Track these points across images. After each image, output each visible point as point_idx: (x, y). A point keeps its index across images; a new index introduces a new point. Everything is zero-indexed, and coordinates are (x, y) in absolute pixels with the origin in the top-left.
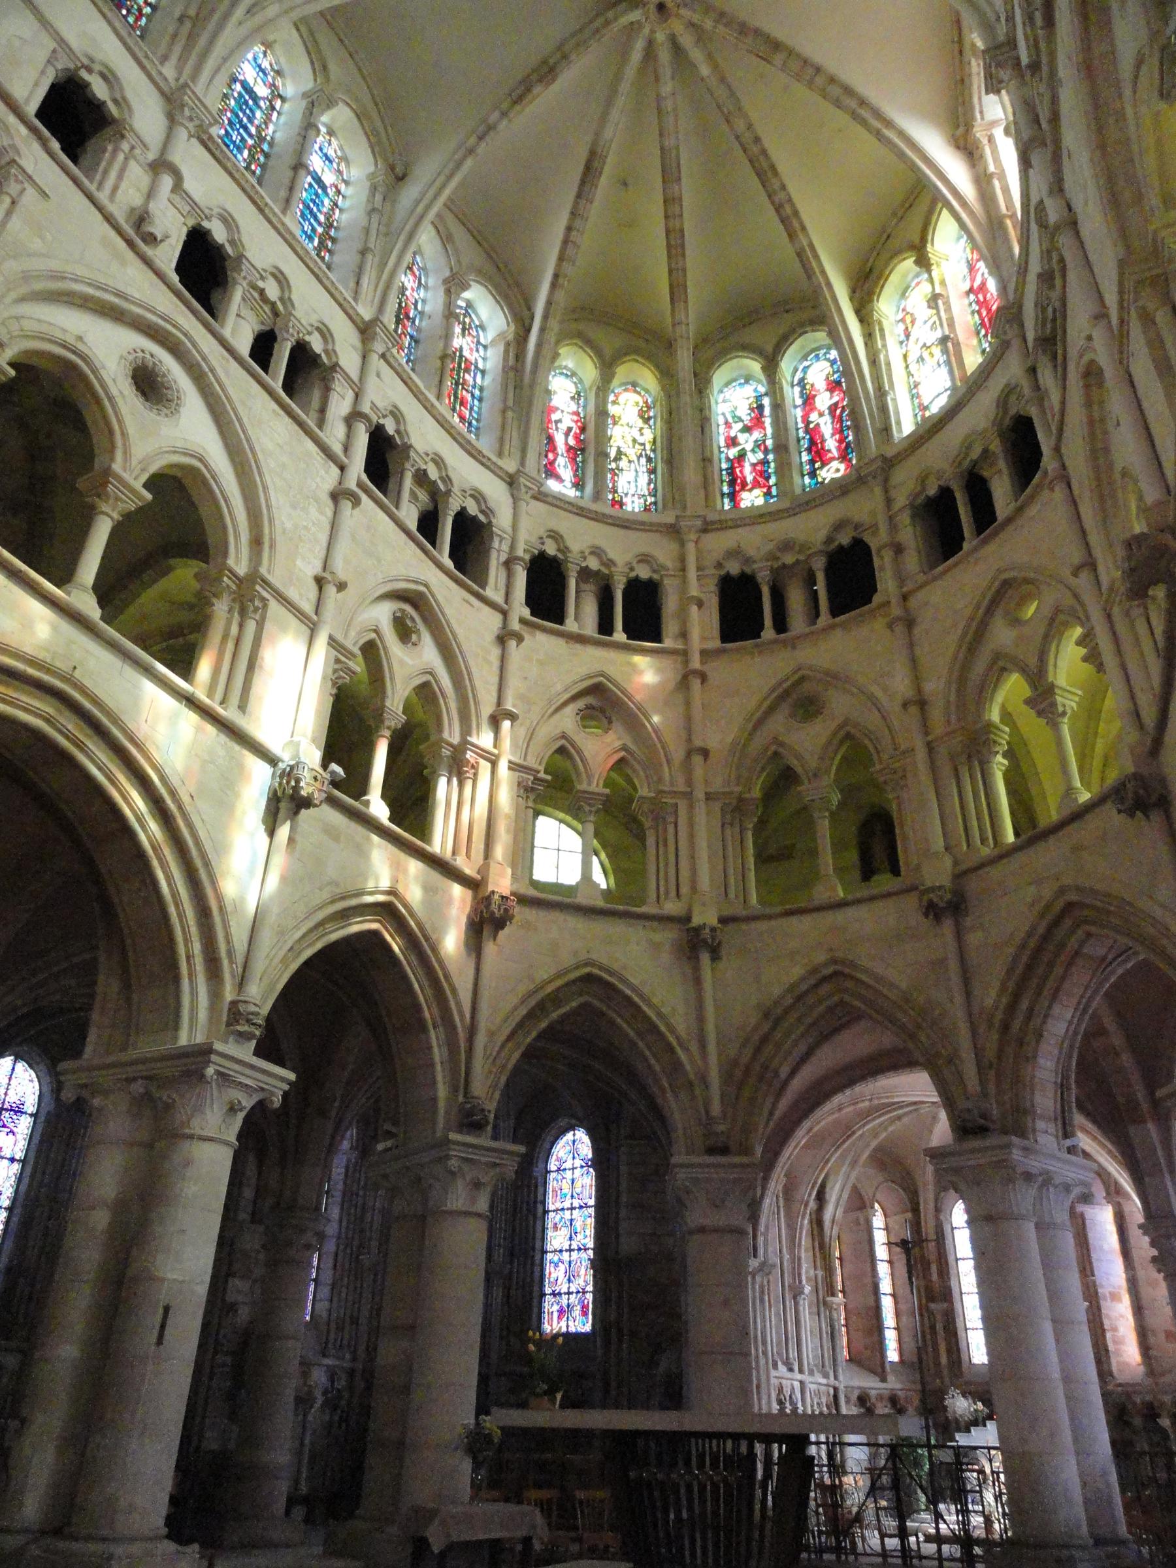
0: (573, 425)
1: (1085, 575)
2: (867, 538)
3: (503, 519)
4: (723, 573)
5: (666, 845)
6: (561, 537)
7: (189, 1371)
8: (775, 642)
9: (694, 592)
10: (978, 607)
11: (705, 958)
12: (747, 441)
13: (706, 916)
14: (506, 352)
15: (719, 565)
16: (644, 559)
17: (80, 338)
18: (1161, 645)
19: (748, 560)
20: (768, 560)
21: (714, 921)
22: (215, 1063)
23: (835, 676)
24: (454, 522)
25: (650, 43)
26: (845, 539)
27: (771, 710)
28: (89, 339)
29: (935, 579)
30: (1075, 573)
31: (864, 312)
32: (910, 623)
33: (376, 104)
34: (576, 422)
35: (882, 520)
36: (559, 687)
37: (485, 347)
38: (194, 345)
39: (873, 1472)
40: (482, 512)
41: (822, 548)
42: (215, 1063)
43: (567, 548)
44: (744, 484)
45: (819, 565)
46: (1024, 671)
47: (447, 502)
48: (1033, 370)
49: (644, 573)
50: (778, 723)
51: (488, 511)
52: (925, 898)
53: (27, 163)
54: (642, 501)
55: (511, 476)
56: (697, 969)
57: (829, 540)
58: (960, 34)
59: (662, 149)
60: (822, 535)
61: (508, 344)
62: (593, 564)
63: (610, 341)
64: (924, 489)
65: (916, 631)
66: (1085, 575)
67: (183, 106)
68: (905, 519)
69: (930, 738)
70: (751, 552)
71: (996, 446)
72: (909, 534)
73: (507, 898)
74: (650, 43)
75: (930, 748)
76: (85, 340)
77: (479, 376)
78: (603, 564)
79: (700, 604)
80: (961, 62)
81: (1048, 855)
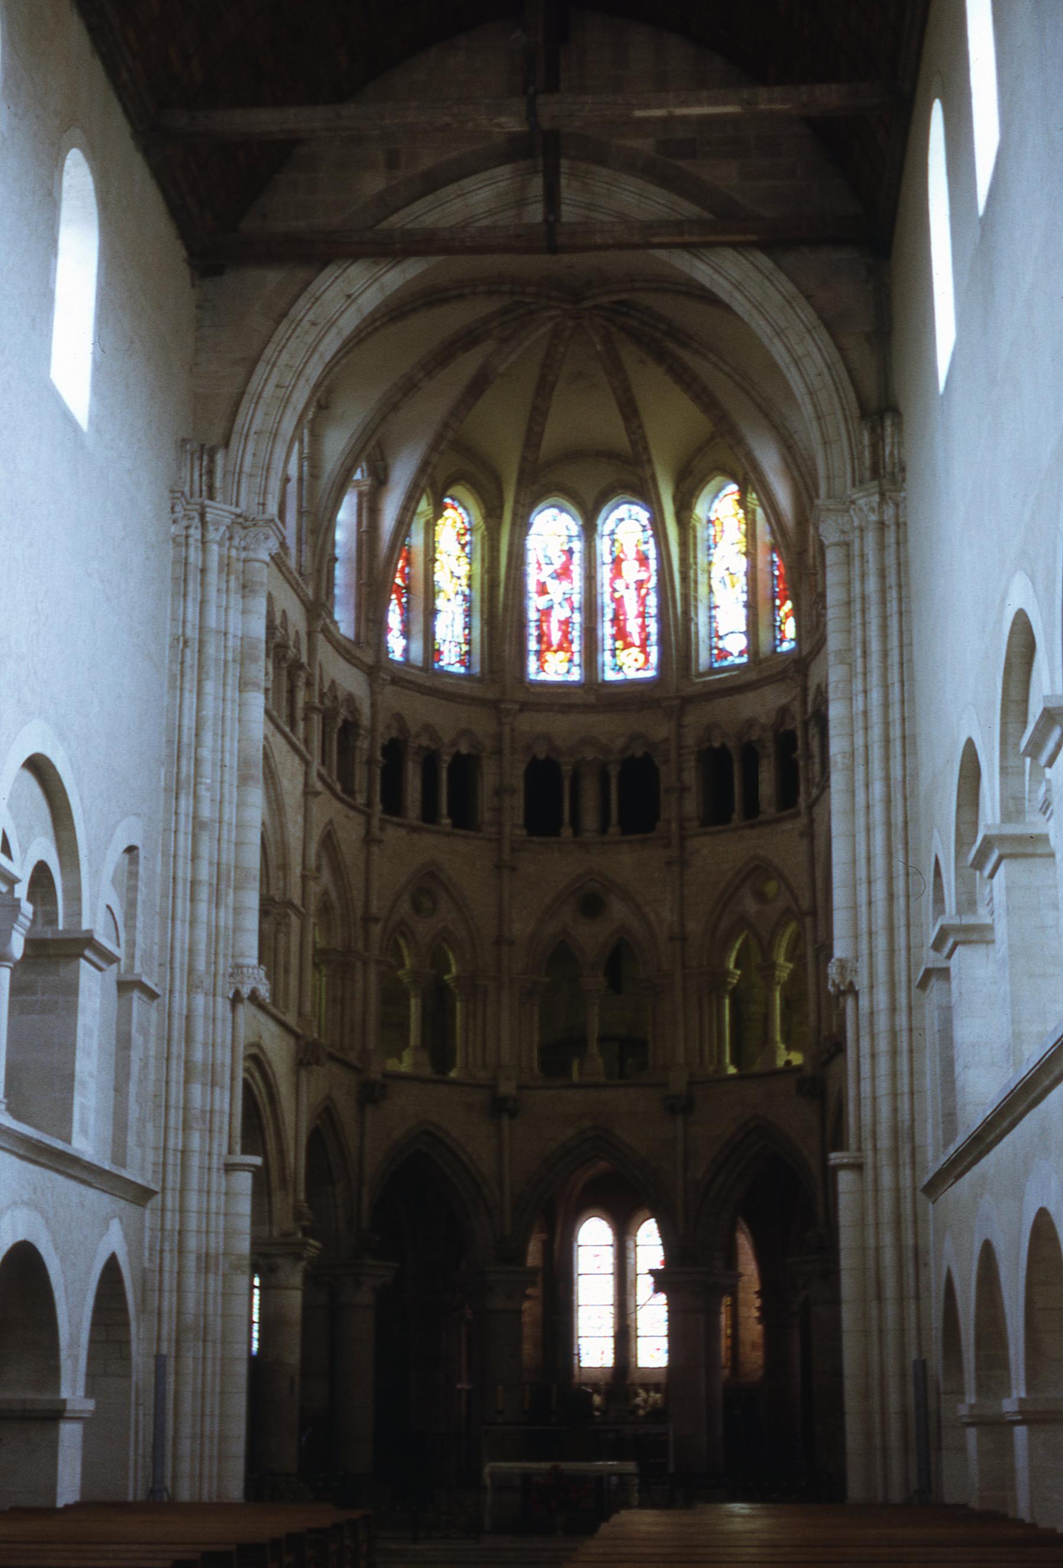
11: (505, 1119)
12: (557, 589)
13: (507, 1088)
16: (465, 733)
18: (935, 832)
39: (855, 617)
44: (549, 645)
45: (614, 771)
54: (458, 649)
55: (371, 668)
60: (620, 743)
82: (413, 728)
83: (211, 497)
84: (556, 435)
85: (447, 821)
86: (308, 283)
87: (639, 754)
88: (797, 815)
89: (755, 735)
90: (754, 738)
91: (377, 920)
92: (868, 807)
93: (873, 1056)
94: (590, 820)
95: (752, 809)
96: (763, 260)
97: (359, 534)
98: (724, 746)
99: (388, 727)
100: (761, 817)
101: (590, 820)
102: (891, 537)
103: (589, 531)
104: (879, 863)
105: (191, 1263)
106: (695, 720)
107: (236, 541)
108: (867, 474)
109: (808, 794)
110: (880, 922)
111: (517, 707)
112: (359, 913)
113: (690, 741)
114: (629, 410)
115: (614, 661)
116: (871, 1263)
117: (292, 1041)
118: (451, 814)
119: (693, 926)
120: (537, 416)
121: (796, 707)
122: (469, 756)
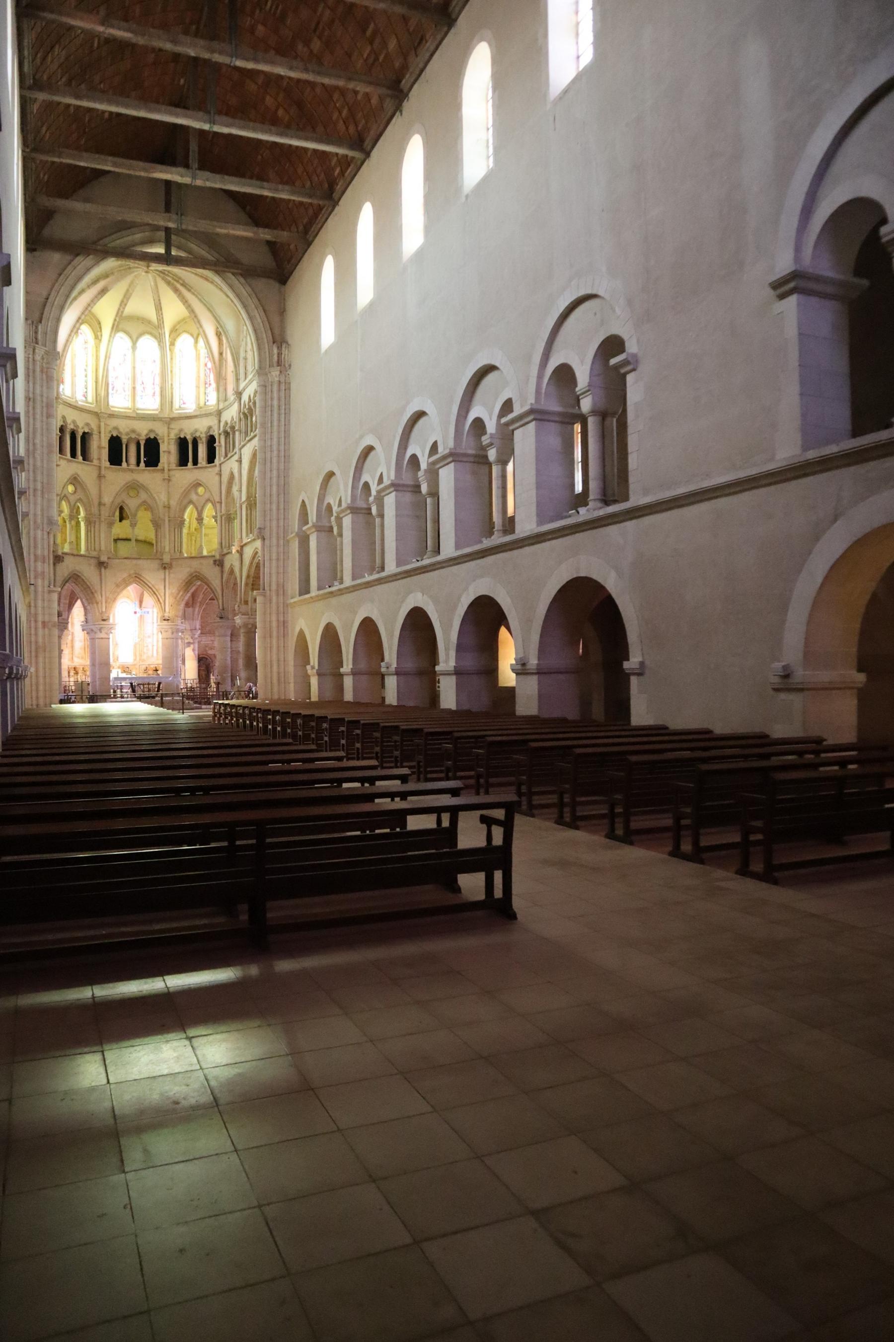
5: (91, 532)
7: (497, 555)
10: (189, 486)
11: (103, 570)
13: (104, 558)
15: (110, 431)
16: (87, 424)
19: (120, 433)
23: (144, 487)
29: (179, 470)
31: (172, 344)
32: (169, 480)
45: (142, 443)
50: (124, 496)
56: (100, 571)
57: (147, 435)
65: (170, 483)
68: (173, 442)
70: (121, 430)
73: (194, 596)
75: (169, 521)
78: (75, 426)
81: (195, 564)
82: (69, 421)
83: (37, 343)
84: (129, 309)
85: (81, 458)
86: (72, 261)
87: (152, 437)
88: (216, 466)
89: (197, 435)
90: (197, 436)
92: (271, 478)
93: (270, 560)
95: (195, 462)
96: (242, 280)
98: (185, 438)
99: (60, 420)
100: (199, 465)
101: (133, 459)
102: (283, 387)
103: (134, 347)
104: (275, 498)
105: (40, 625)
106: (176, 426)
107: (45, 361)
108: (275, 364)
109: (220, 459)
110: (275, 517)
111: (106, 416)
113: (173, 436)
114: (159, 308)
115: (85, 378)
116: (268, 626)
118: (82, 455)
119: (173, 503)
120: (123, 304)
121: (216, 428)
122: (88, 433)
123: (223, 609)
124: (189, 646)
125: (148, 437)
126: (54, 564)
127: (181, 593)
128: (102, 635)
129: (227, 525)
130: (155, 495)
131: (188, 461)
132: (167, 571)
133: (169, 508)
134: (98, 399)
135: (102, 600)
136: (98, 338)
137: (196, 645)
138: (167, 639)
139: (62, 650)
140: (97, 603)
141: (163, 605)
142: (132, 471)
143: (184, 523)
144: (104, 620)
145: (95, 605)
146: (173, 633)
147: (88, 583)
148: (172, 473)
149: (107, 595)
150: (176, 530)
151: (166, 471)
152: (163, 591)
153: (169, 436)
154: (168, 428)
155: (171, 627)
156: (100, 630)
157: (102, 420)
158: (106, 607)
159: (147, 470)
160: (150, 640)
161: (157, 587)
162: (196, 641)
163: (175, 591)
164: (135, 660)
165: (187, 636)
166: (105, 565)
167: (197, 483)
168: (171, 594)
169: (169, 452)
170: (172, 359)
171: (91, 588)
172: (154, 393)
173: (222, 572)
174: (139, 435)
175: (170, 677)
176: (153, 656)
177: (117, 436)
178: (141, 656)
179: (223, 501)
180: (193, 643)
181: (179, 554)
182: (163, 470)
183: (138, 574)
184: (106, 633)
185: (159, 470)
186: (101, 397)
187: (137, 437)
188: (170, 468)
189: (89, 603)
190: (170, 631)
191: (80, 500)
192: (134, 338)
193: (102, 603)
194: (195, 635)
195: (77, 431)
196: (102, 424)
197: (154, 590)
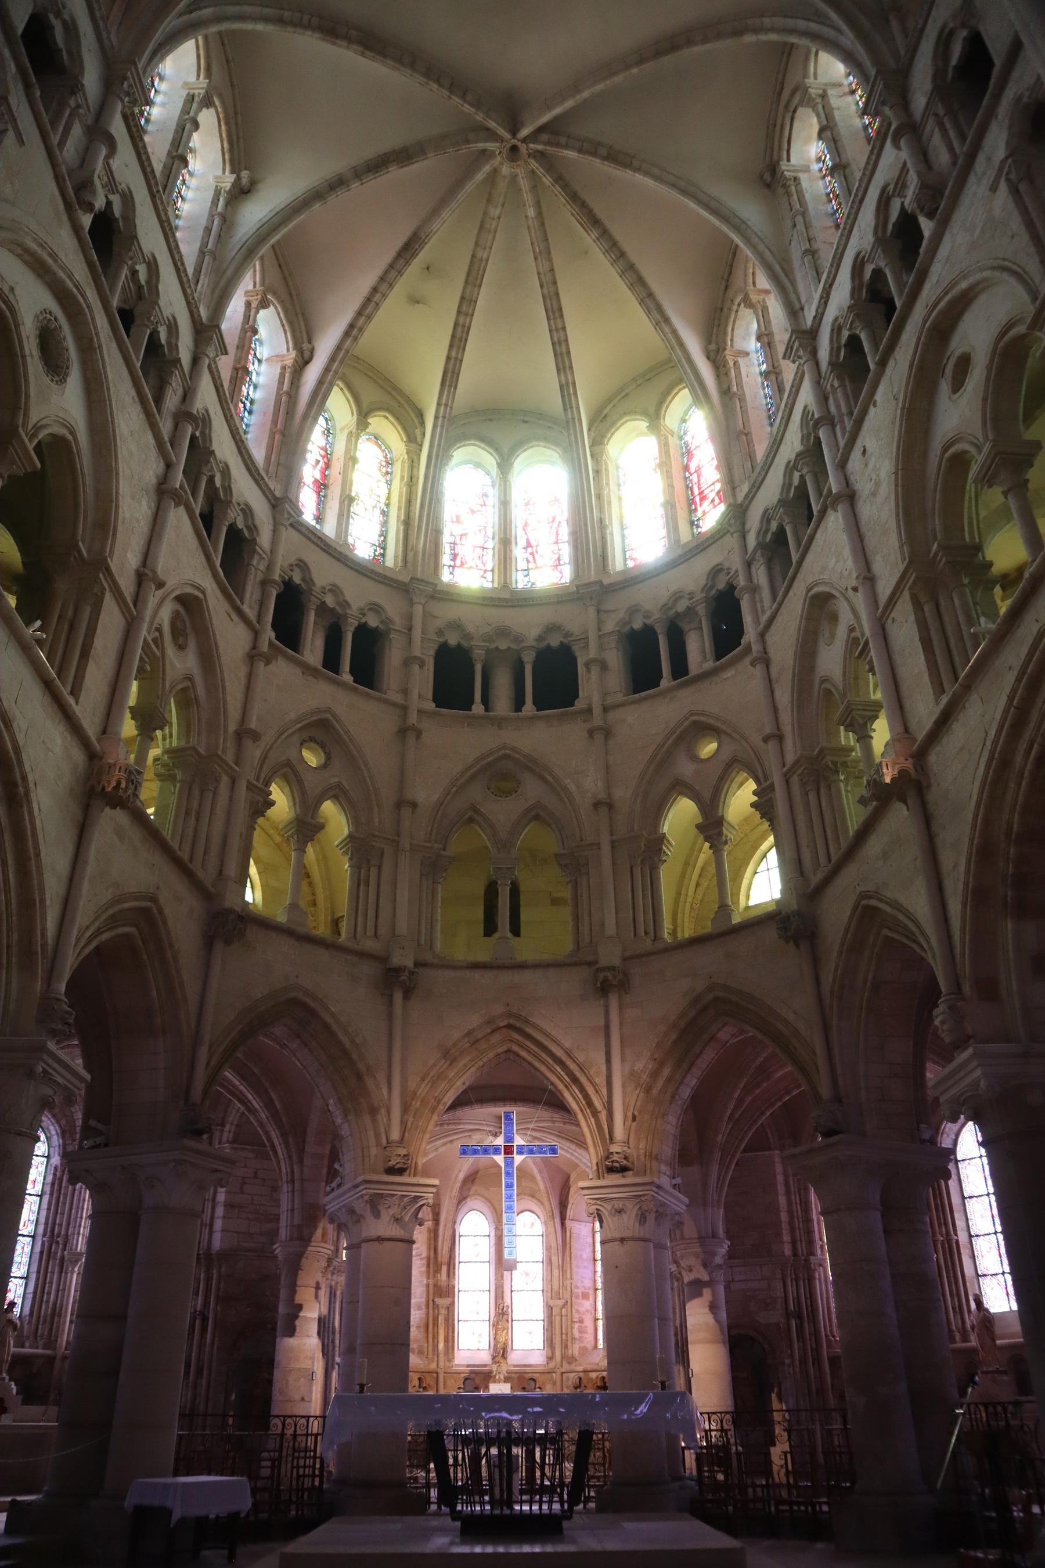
0: (320, 459)
1: (772, 745)
2: (576, 648)
3: (264, 539)
4: (442, 640)
6: (308, 568)
8: (482, 717)
9: (417, 653)
11: (398, 996)
13: (402, 958)
14: (282, 375)
15: (440, 632)
16: (375, 608)
17: (12, 289)
20: (484, 641)
21: (410, 964)
22: (45, 1062)
24: (227, 531)
25: (495, 171)
26: (555, 641)
27: (473, 777)
28: (18, 291)
29: (634, 702)
30: (766, 740)
32: (607, 733)
33: (236, 113)
34: (323, 457)
35: (592, 635)
36: (292, 716)
37: (260, 361)
38: (93, 319)
40: (248, 527)
41: (534, 644)
42: (45, 1062)
43: (312, 580)
45: (529, 658)
46: (696, 797)
47: (226, 513)
48: (749, 565)
49: (373, 622)
51: (253, 528)
52: (601, 975)
53: (13, 101)
56: (390, 1004)
57: (540, 638)
58: (730, 273)
59: (473, 256)
60: (535, 632)
61: (284, 368)
62: (330, 601)
63: (370, 394)
64: (629, 622)
66: (772, 745)
67: (125, 79)
69: (614, 838)
70: (470, 628)
71: (701, 610)
72: (615, 658)
74: (495, 171)
75: (613, 845)
76: (16, 292)
77: (252, 388)
79: (422, 665)
80: (724, 297)
85: (347, 677)
91: (255, 736)
94: (502, 703)
95: (680, 668)
97: (279, 395)
101: (502, 703)
112: (232, 727)
117: (79, 756)
119: (622, 794)
123: (839, 1100)
124: (699, 1294)
125: (544, 644)
126: (209, 942)
127: (666, 1072)
128: (384, 1227)
129: (812, 796)
130: (567, 781)
131: (661, 677)
132: (614, 1000)
133: (611, 806)
134: (410, 555)
135: (390, 1098)
136: (413, 440)
137: (721, 1290)
138: (622, 1240)
139: (300, 1307)
140: (373, 1111)
141: (603, 1116)
142: (499, 722)
143: (660, 850)
144: (391, 1171)
145: (367, 1120)
146: (642, 1218)
147: (345, 1040)
148: (612, 715)
149: (412, 1085)
150: (638, 871)
151: (597, 710)
152: (604, 1068)
153: (599, 630)
154: (598, 611)
155: (638, 1191)
156: (375, 1203)
157: (416, 600)
158: (404, 1124)
159: (540, 718)
160: (587, 1304)
161: (581, 1057)
162: (720, 1276)
163: (643, 1064)
164: (550, 1358)
165: (691, 1261)
166: (404, 977)
167: (695, 722)
168: (632, 1076)
169: (604, 666)
170: (597, 472)
171: (355, 1056)
172: (559, 559)
173: (816, 963)
174: (518, 639)
175: (638, 1400)
176: (596, 1347)
177: (459, 646)
178: (566, 1347)
179: (787, 730)
180: (710, 1284)
181: (649, 942)
182: (589, 711)
183: (518, 1017)
184: (397, 1220)
185: (575, 713)
186: (416, 554)
187: (513, 646)
188: (609, 701)
189: (346, 1116)
190: (632, 1212)
191: (338, 794)
192: (506, 450)
193: (389, 1112)
194: (714, 1254)
195: (346, 616)
196: (418, 610)
197: (572, 1066)
